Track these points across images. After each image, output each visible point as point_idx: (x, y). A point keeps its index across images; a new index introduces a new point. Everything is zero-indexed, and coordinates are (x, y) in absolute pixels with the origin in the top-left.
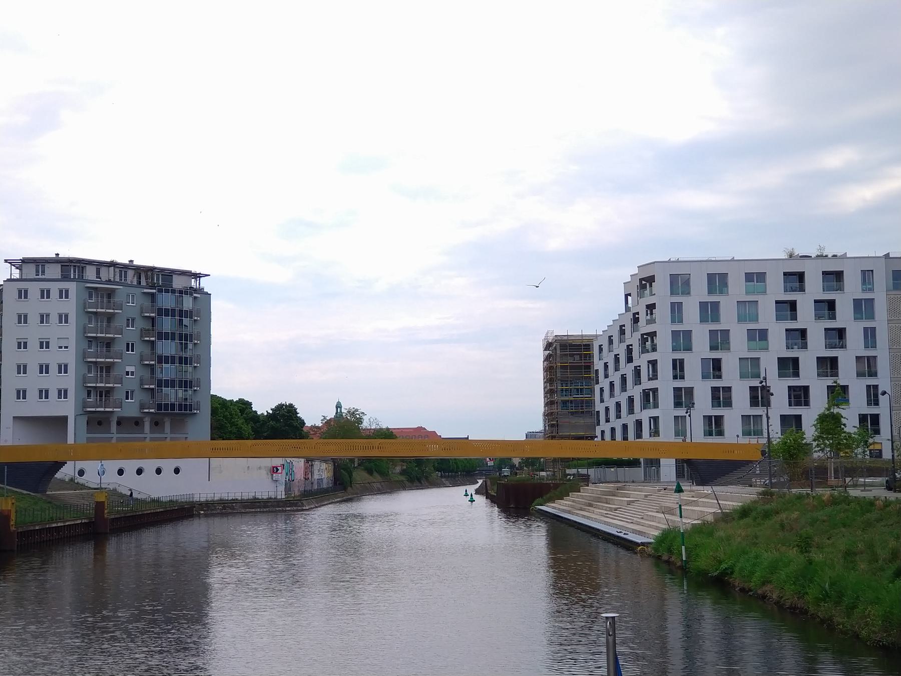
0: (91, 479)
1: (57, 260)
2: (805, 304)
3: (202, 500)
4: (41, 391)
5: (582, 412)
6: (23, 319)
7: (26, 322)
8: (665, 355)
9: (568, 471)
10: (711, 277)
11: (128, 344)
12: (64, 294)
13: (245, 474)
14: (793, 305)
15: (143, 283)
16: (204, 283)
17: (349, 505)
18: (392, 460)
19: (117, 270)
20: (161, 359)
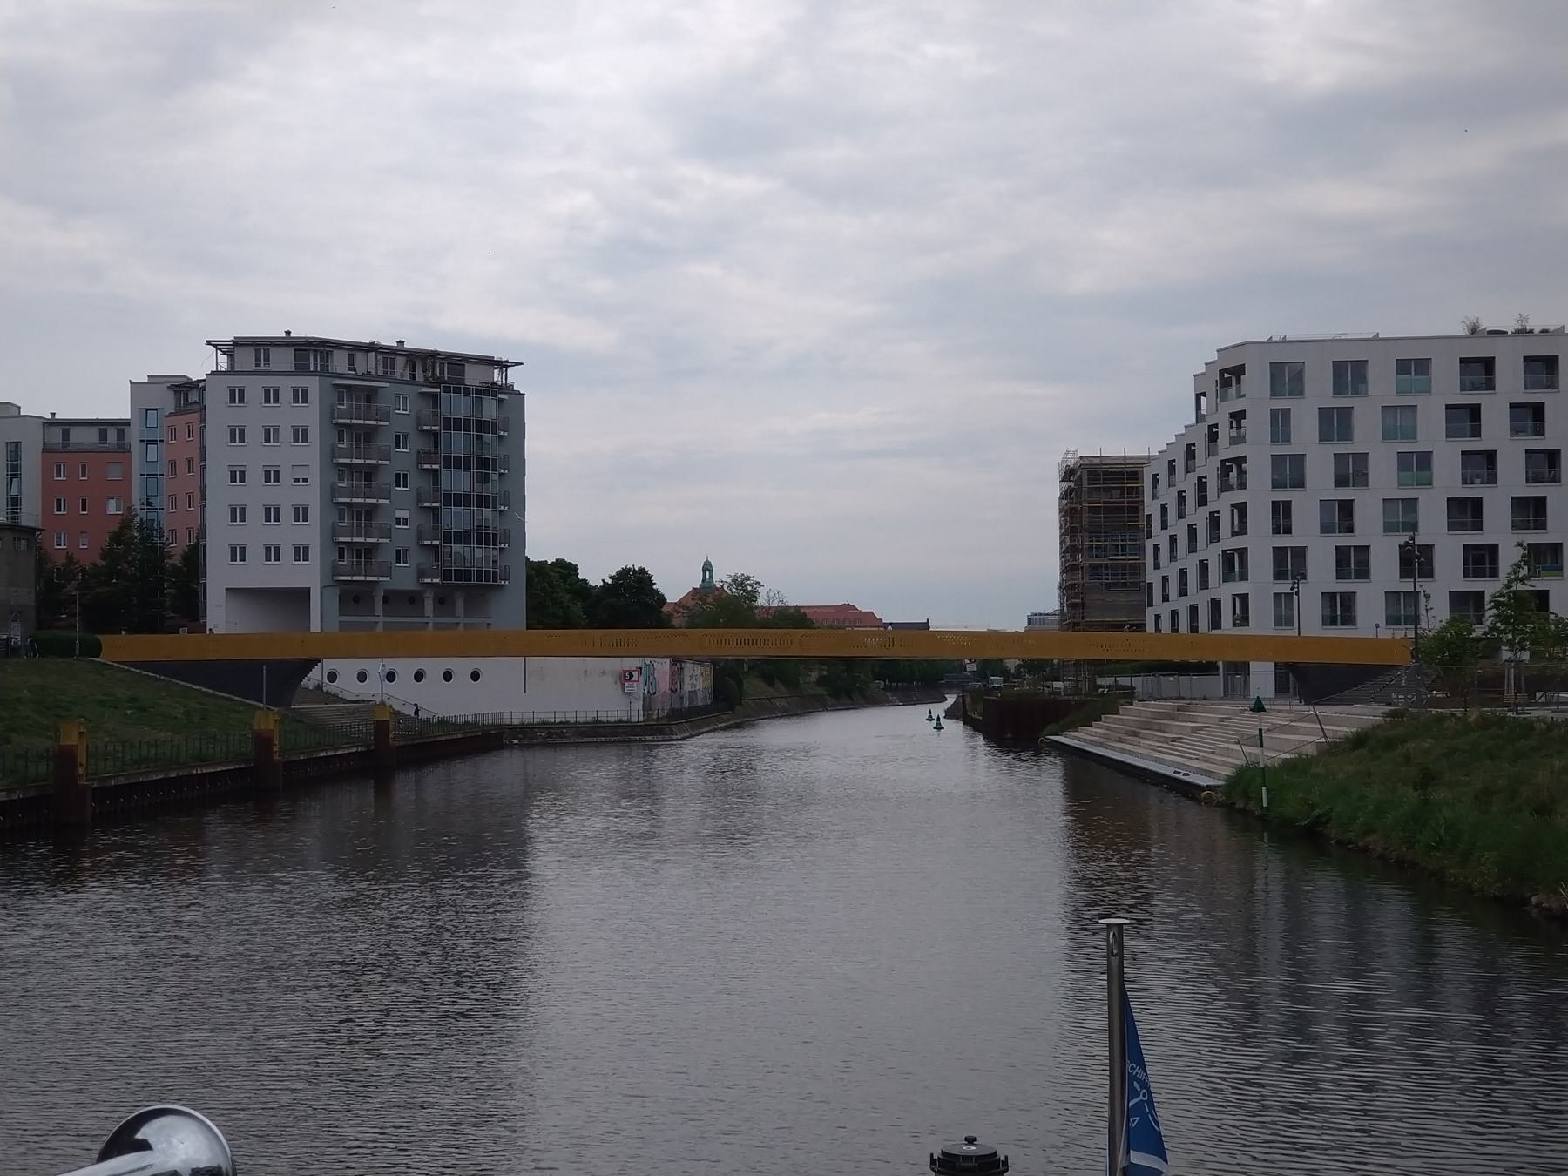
0: (346, 685)
1: (287, 342)
2: (1495, 410)
3: (515, 722)
4: (268, 549)
5: (1125, 585)
6: (237, 434)
7: (242, 440)
8: (1259, 494)
9: (1100, 681)
10: (1339, 367)
11: (398, 476)
12: (300, 395)
14: (1474, 412)
15: (420, 377)
16: (515, 377)
17: (736, 733)
18: (807, 662)
19: (380, 357)
20: (449, 500)
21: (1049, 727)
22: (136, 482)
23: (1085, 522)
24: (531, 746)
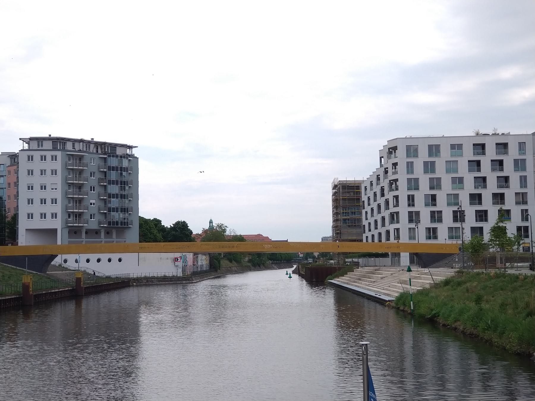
1: (50, 139)
8: (403, 192)
10: (430, 147)
11: (91, 187)
12: (54, 158)
13: (159, 262)
15: (100, 152)
16: (135, 152)
18: (243, 254)
21: (329, 277)
23: (341, 203)
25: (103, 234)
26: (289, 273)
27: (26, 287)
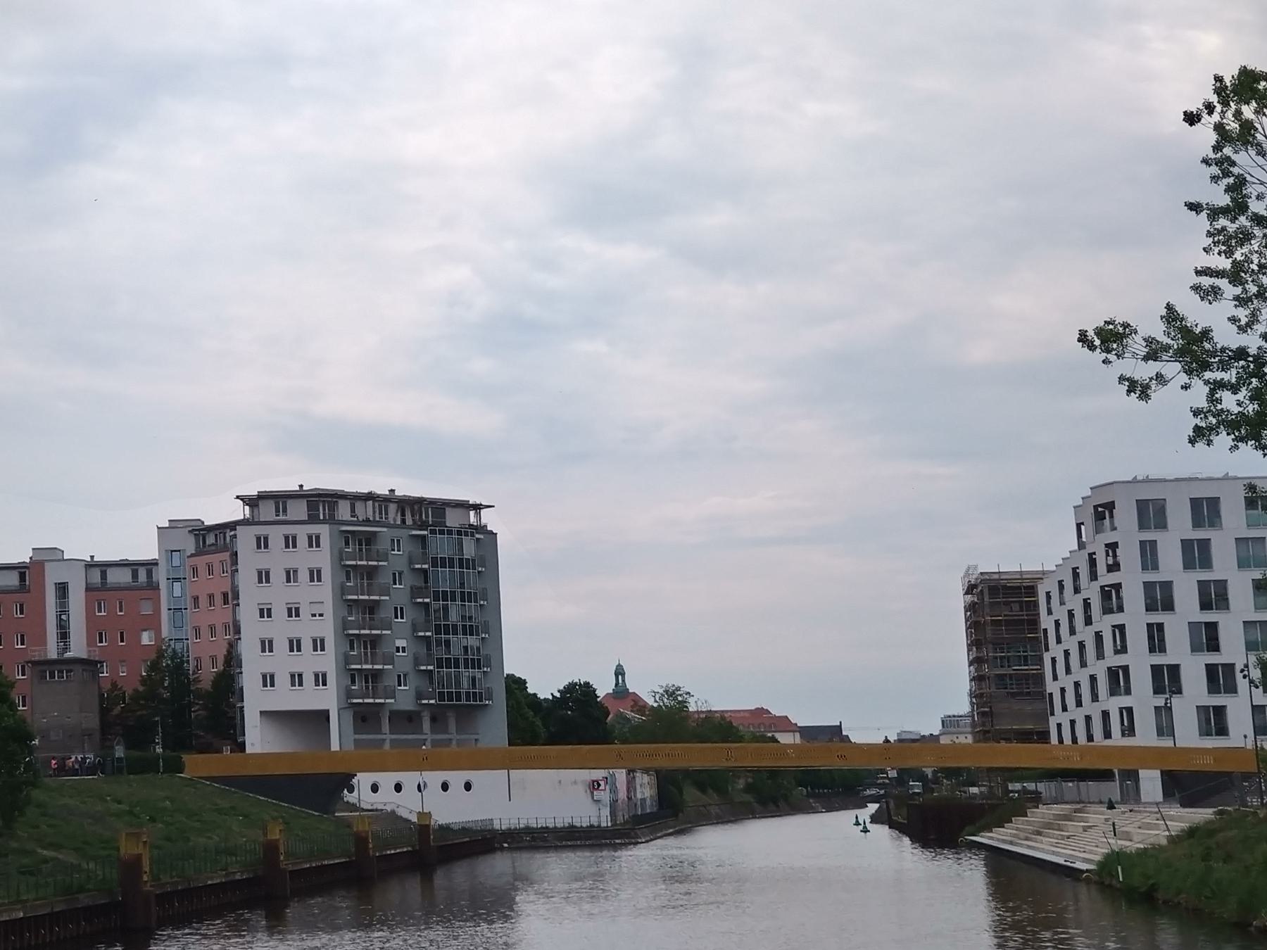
8: (1135, 617)
10: (1196, 503)
11: (396, 609)
12: (314, 541)
13: (555, 792)
15: (409, 522)
16: (488, 518)
18: (736, 772)
21: (967, 829)
22: (165, 615)
23: (989, 635)
24: (520, 849)
25: (426, 725)
26: (861, 822)
27: (271, 848)
